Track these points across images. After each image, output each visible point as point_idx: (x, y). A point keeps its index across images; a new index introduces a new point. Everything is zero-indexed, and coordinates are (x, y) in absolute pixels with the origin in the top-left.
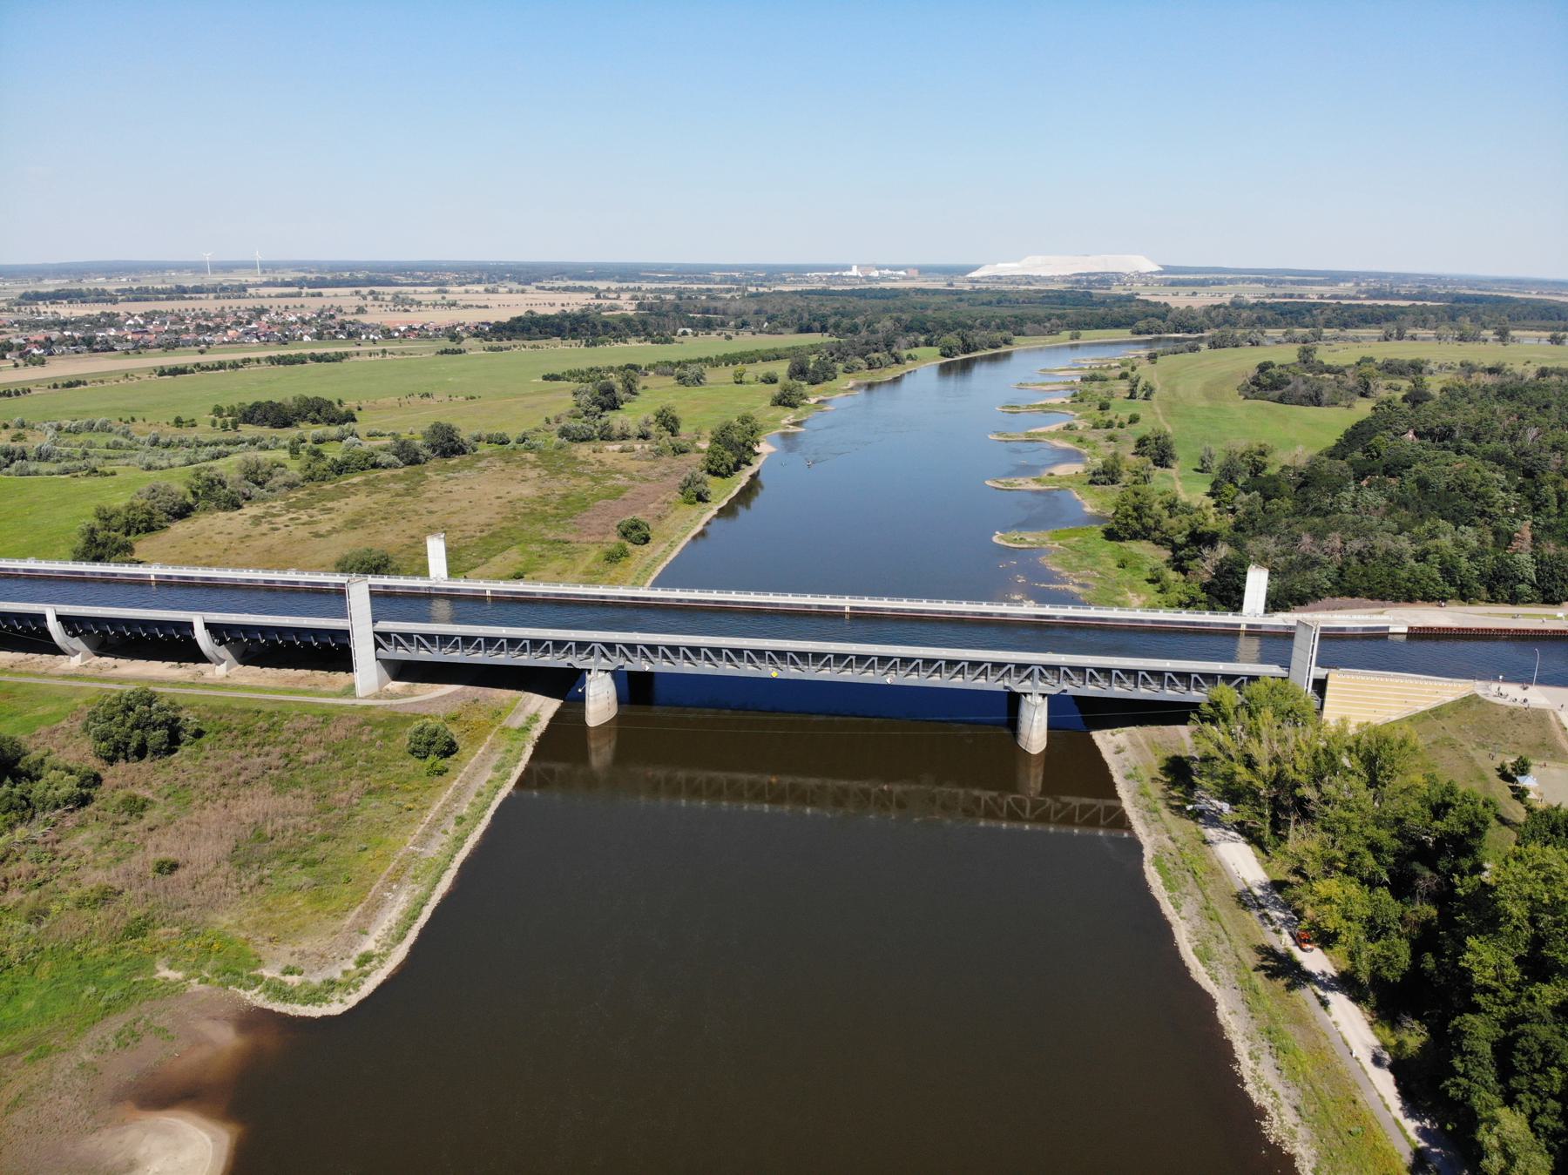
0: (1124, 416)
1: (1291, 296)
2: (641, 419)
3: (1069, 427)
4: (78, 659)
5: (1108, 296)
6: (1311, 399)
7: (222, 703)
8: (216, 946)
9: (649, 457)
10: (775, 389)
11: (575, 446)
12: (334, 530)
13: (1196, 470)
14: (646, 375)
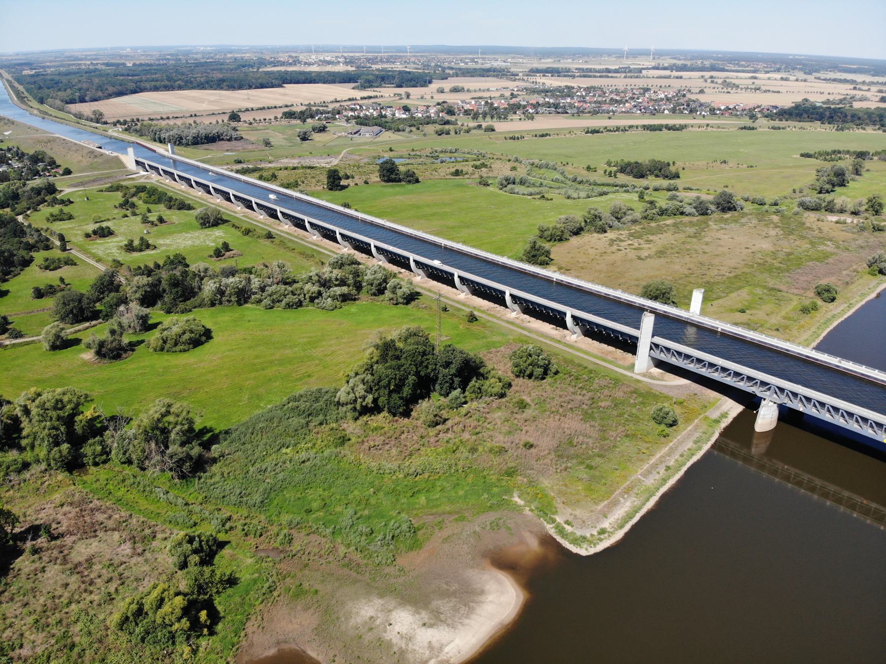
2: (857, 201)
4: (514, 313)
7: (569, 357)
8: (540, 496)
9: (855, 230)
11: (807, 214)
12: (649, 257)
14: (872, 159)
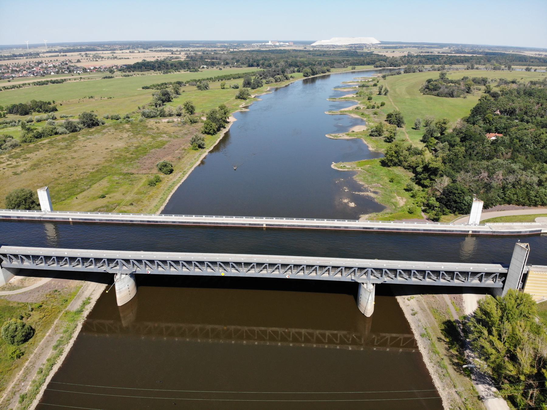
0: (379, 103)
1: (428, 52)
2: (177, 108)
3: (357, 108)
5: (363, 53)
6: (450, 95)
9: (180, 125)
10: (237, 92)
12: (25, 171)
13: (413, 128)
14: (185, 86)
